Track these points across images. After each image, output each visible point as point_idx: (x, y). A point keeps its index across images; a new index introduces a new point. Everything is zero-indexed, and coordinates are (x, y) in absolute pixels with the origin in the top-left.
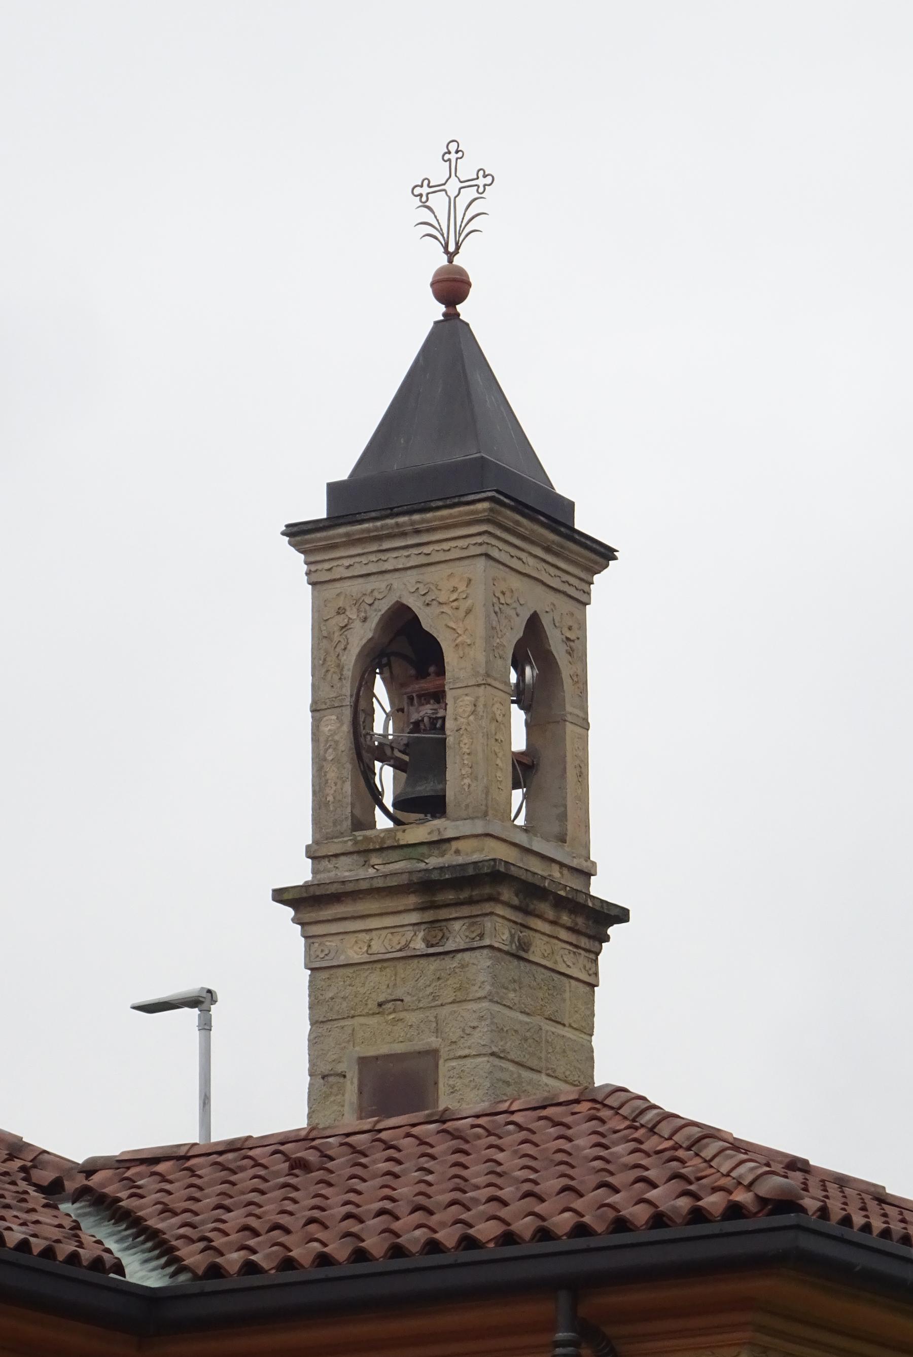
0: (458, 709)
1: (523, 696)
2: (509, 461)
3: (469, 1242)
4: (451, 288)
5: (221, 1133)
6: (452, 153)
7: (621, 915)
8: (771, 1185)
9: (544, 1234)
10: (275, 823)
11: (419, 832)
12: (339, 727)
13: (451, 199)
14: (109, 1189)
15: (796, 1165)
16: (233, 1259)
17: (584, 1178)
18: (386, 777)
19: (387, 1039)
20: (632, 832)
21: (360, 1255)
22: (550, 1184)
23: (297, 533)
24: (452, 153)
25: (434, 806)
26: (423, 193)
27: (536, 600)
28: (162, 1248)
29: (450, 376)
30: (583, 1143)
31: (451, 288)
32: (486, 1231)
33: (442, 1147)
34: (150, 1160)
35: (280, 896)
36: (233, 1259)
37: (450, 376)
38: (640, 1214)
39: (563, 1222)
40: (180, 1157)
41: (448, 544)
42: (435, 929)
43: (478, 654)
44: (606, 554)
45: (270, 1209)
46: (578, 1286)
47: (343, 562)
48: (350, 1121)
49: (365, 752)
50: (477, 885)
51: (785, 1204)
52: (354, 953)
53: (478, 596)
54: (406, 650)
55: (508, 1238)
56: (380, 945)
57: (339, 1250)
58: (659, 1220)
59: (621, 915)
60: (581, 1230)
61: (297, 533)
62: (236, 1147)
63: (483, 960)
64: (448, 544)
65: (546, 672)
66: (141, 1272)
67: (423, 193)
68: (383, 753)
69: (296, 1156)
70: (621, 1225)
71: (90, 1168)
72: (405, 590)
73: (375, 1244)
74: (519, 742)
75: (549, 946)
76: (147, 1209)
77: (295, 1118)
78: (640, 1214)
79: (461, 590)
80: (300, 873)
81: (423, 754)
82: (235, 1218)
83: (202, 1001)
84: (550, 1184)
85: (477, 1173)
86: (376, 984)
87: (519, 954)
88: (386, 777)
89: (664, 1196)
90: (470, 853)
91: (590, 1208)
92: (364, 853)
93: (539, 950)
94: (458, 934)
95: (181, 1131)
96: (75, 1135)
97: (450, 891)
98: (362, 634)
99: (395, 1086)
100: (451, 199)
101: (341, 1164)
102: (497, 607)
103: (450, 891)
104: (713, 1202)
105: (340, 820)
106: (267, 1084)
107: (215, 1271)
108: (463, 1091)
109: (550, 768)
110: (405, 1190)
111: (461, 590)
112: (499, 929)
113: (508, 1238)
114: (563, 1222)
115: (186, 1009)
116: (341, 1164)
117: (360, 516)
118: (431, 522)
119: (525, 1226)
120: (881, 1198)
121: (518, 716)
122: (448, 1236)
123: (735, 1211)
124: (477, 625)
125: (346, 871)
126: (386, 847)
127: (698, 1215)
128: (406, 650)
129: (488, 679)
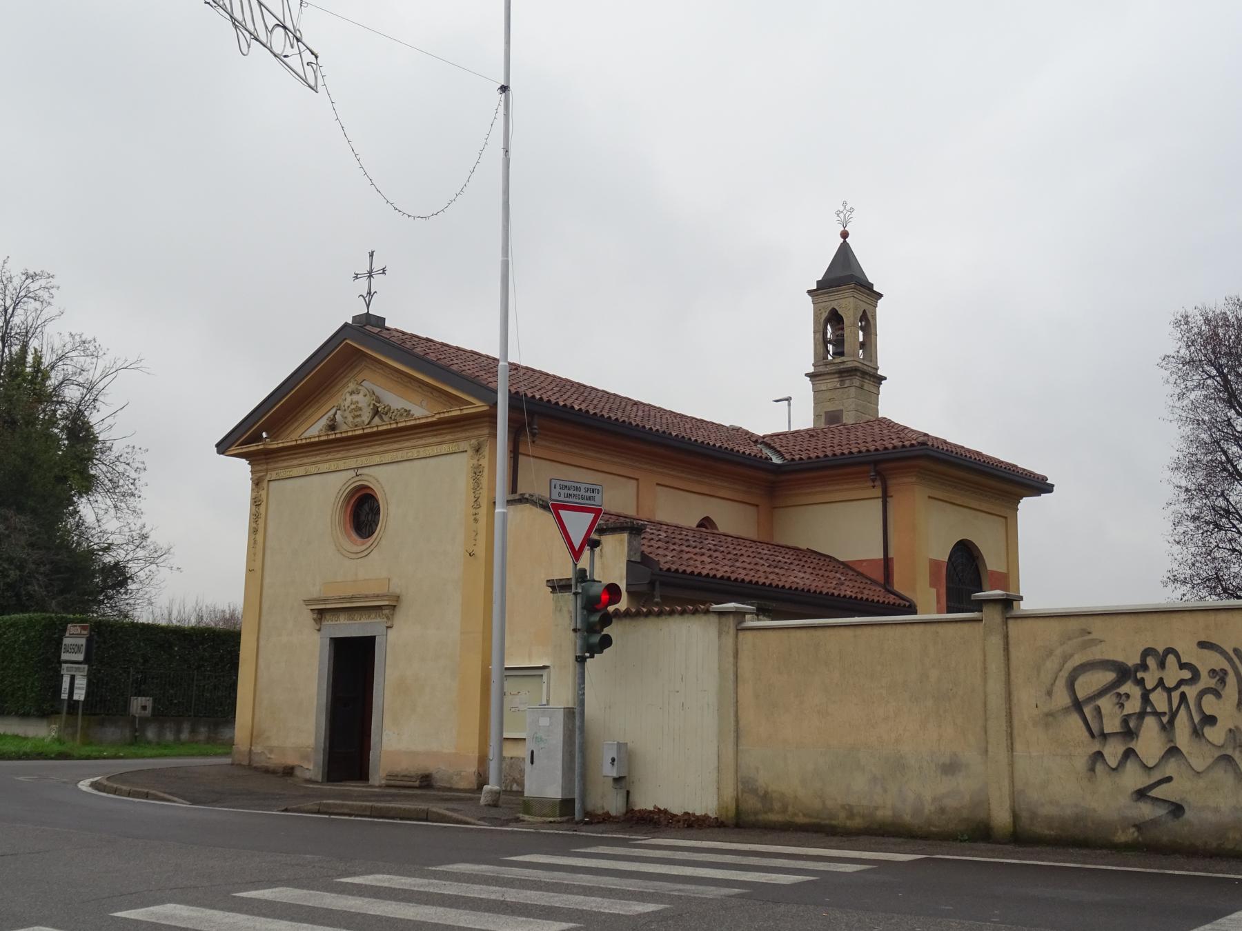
0: (847, 332)
1: (862, 328)
2: (858, 275)
3: (851, 453)
4: (845, 235)
5: (793, 429)
6: (845, 204)
7: (885, 378)
8: (920, 439)
9: (868, 451)
10: (806, 360)
11: (839, 360)
12: (820, 336)
13: (845, 215)
14: (768, 442)
15: (926, 435)
16: (797, 457)
17: (877, 438)
18: (830, 347)
19: (831, 407)
20: (886, 361)
21: (826, 456)
22: (869, 439)
23: (810, 292)
24: (845, 204)
25: (842, 354)
26: (838, 213)
27: (865, 306)
28: (781, 455)
29: (845, 256)
30: (877, 430)
31: (845, 235)
32: (855, 450)
33: (844, 431)
34: (777, 435)
35: (224, 447)
36: (797, 457)
37: (845, 256)
38: (890, 446)
39: (872, 448)
40: (784, 434)
41: (844, 292)
42: (842, 382)
43: (852, 319)
44: (881, 296)
45: (805, 446)
46: (876, 463)
47: (821, 298)
48: (823, 426)
49: (826, 342)
50: (851, 372)
51: (924, 444)
52: (824, 388)
53: (852, 306)
54: (835, 318)
55: (860, 452)
56: (830, 386)
57: (821, 455)
58: (895, 447)
59: (885, 378)
60: (877, 450)
61: (810, 292)
62: (796, 432)
63: (853, 389)
64: (844, 292)
65: (867, 322)
66: (776, 460)
67: (838, 213)
68: (830, 342)
69: (811, 434)
70: (886, 448)
71: (764, 437)
72: (834, 305)
73: (830, 454)
74: (861, 339)
75: (868, 386)
76: (777, 446)
77: (811, 426)
78: (890, 446)
79: (847, 305)
80: (811, 370)
81: (839, 342)
82: (797, 448)
83: (788, 399)
84: (869, 439)
85: (852, 437)
86: (828, 395)
87: (861, 387)
88: (830, 347)
89: (896, 442)
90: (850, 365)
91: (878, 445)
92: (826, 365)
93: (866, 387)
94: (847, 383)
95: (785, 429)
96: (761, 430)
97: (845, 373)
98: (825, 315)
99: (833, 418)
100: (845, 215)
101: (821, 435)
102: (856, 308)
103: (845, 373)
104: (907, 443)
105: (820, 357)
106: (803, 418)
107: (793, 460)
108: (849, 418)
109: (868, 345)
110: (836, 441)
111: (847, 305)
112: (857, 382)
113: (860, 452)
114: (872, 448)
115: (677, 810)
116: (821, 435)
117: (824, 288)
118: (543, 823)
119: (864, 449)
120: (946, 442)
121: (861, 333)
122: (846, 452)
123: (912, 445)
124: (851, 312)
125: (822, 369)
126: (831, 363)
127: (903, 446)
128: (835, 318)
129: (854, 324)
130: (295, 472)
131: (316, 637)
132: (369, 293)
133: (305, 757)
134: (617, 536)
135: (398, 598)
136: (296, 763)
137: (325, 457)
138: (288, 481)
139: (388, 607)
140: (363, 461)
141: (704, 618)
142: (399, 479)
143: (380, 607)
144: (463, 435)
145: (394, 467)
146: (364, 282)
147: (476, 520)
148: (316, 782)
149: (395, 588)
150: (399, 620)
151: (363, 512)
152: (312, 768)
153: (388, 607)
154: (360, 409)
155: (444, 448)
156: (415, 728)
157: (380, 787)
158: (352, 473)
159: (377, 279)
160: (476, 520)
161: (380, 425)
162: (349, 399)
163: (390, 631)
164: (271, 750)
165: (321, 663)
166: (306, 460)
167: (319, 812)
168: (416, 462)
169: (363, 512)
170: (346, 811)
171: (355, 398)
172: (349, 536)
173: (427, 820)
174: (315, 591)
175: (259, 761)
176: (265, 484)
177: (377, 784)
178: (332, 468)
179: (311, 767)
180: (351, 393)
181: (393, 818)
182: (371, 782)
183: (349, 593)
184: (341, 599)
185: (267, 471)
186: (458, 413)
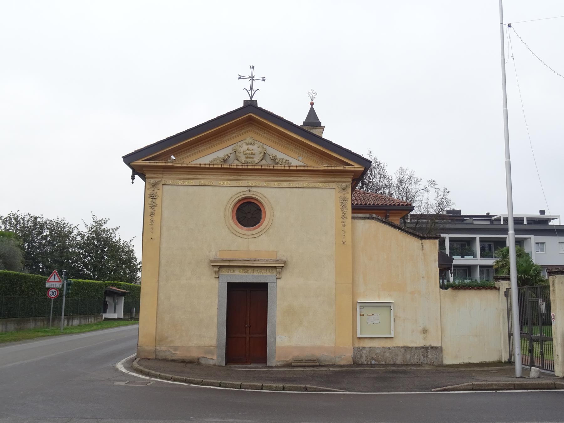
4: (312, 104)
6: (312, 90)
24: (312, 90)
26: (309, 94)
31: (312, 104)
130: (189, 182)
131: (216, 282)
132: (251, 89)
134: (432, 241)
135: (285, 262)
138: (182, 187)
139: (277, 267)
143: (275, 267)
145: (278, 190)
146: (247, 84)
147: (344, 225)
148: (222, 366)
149: (282, 255)
151: (248, 213)
152: (217, 358)
153: (277, 267)
154: (254, 154)
155: (318, 185)
156: (292, 334)
157: (276, 367)
158: (246, 189)
159: (257, 84)
160: (344, 225)
162: (245, 147)
163: (278, 281)
164: (176, 349)
165: (219, 296)
166: (200, 177)
167: (473, 390)
168: (294, 189)
169: (248, 213)
170: (495, 387)
171: (250, 147)
172: (236, 225)
173: (555, 388)
174: (213, 254)
175: (161, 355)
176: (160, 186)
178: (225, 184)
180: (247, 144)
181: (503, 390)
182: (269, 364)
183: (267, 258)
184: (240, 261)
185: (162, 178)
186: (342, 168)
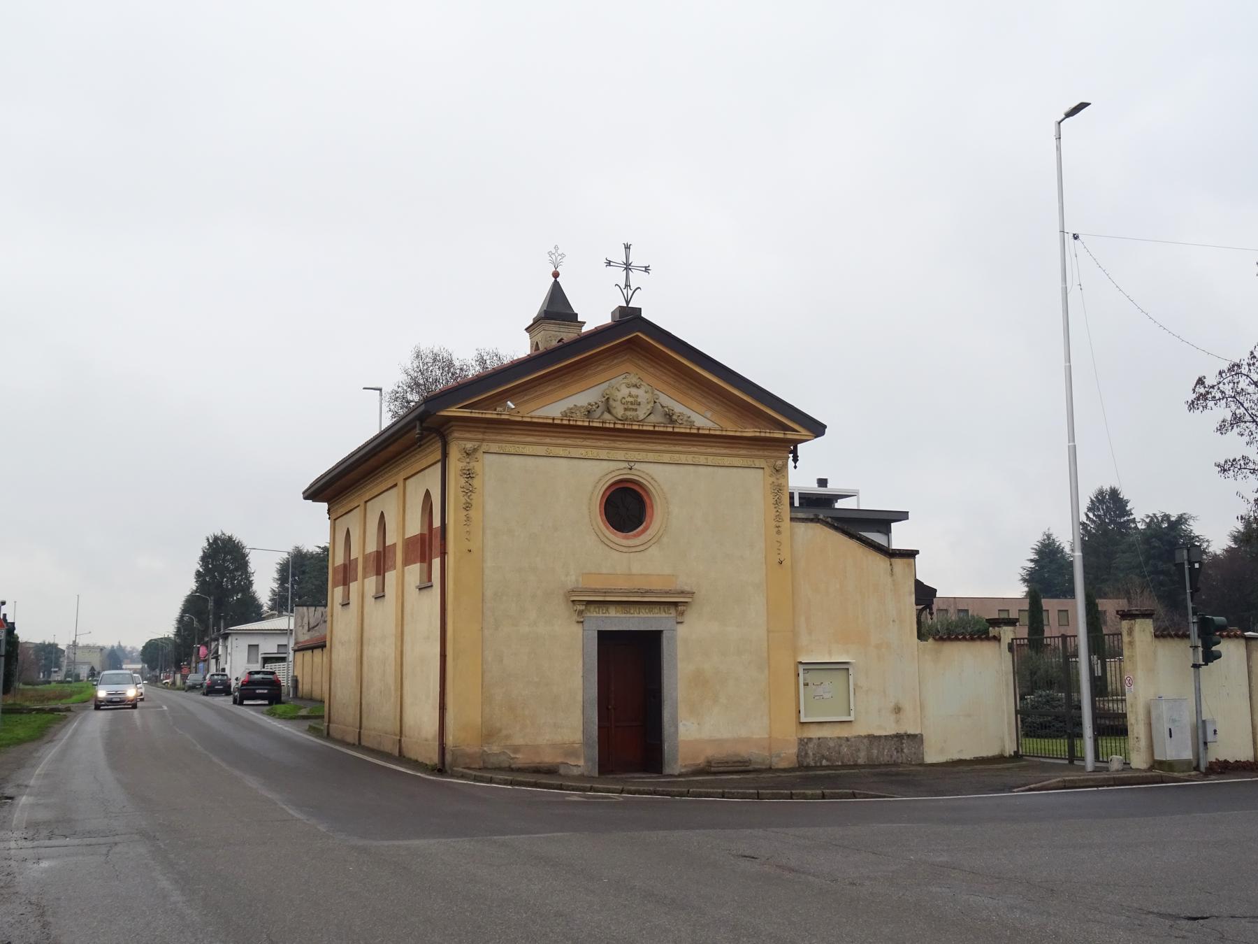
4: (556, 275)
13: (556, 258)
26: (550, 254)
31: (556, 275)
100: (556, 258)
131: (578, 629)
133: (572, 753)
136: (559, 760)
137: (579, 442)
139: (676, 604)
140: (633, 455)
141: (1236, 641)
142: (668, 478)
144: (761, 453)
147: (779, 532)
149: (683, 583)
150: (691, 617)
151: (626, 508)
152: (583, 763)
153: (676, 604)
156: (707, 717)
158: (626, 465)
160: (779, 532)
161: (655, 422)
164: (516, 749)
168: (701, 468)
169: (626, 508)
171: (634, 391)
177: (676, 772)
178: (590, 456)
179: (581, 763)
182: (667, 770)
186: (781, 436)
